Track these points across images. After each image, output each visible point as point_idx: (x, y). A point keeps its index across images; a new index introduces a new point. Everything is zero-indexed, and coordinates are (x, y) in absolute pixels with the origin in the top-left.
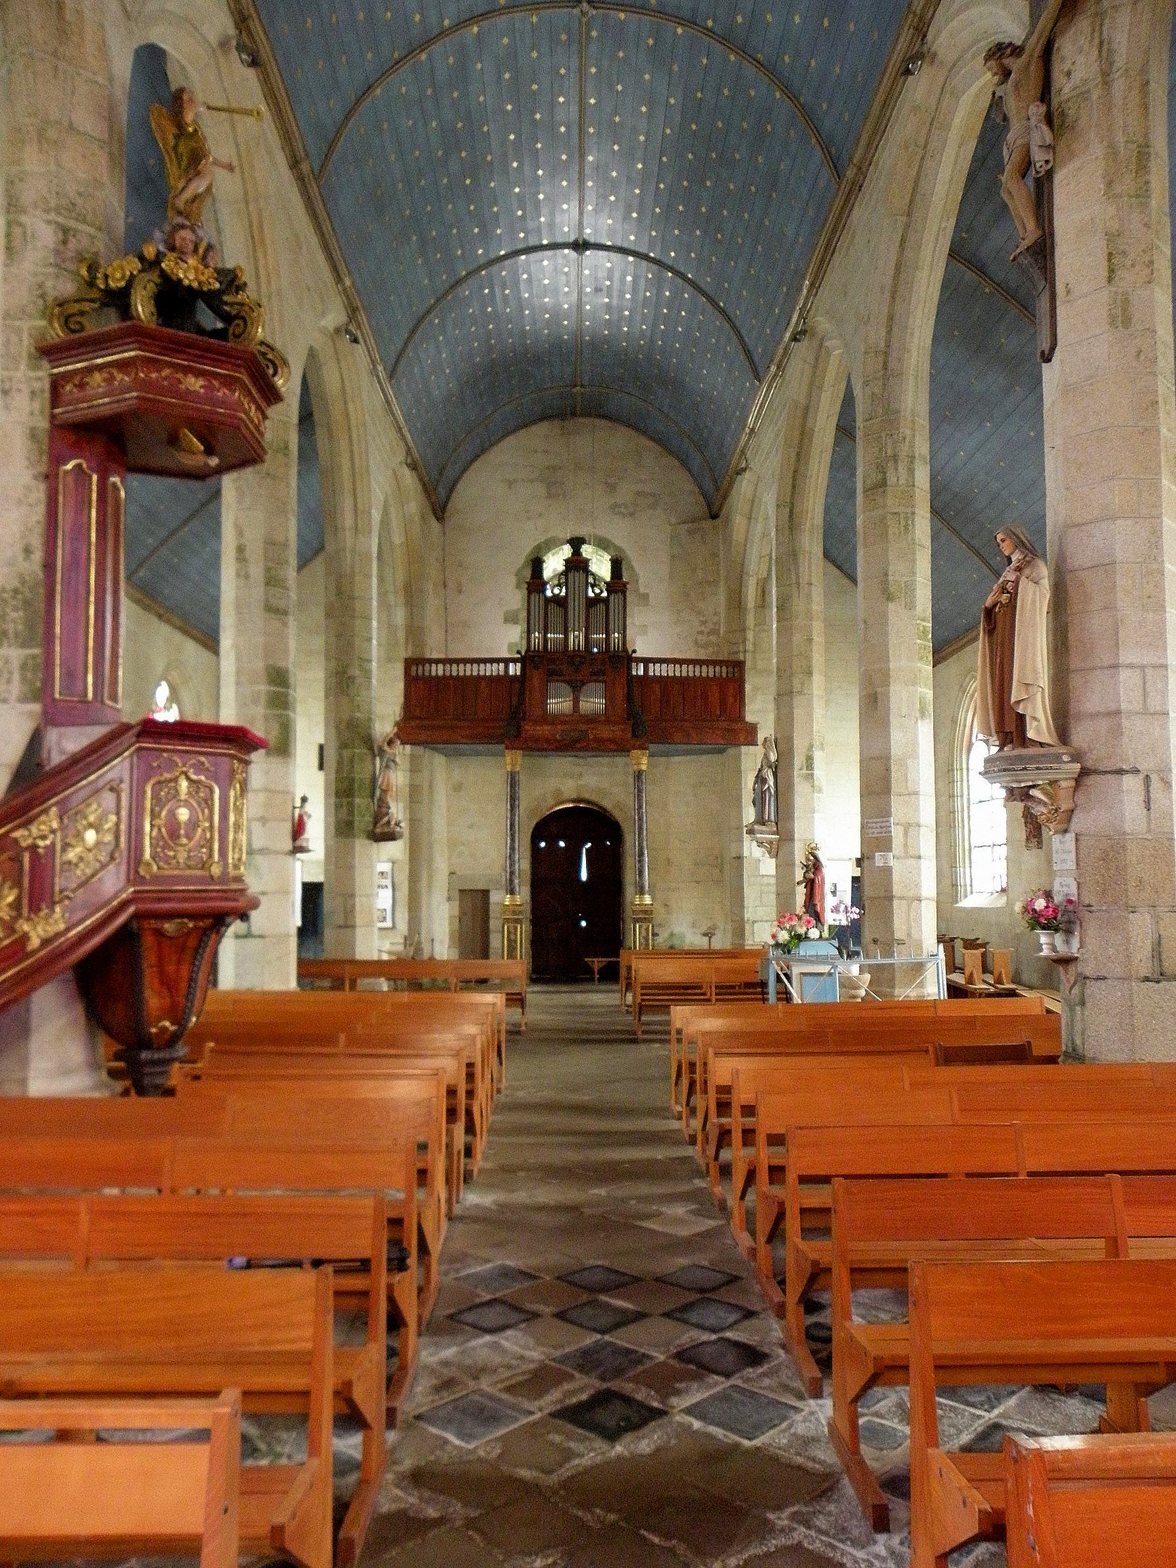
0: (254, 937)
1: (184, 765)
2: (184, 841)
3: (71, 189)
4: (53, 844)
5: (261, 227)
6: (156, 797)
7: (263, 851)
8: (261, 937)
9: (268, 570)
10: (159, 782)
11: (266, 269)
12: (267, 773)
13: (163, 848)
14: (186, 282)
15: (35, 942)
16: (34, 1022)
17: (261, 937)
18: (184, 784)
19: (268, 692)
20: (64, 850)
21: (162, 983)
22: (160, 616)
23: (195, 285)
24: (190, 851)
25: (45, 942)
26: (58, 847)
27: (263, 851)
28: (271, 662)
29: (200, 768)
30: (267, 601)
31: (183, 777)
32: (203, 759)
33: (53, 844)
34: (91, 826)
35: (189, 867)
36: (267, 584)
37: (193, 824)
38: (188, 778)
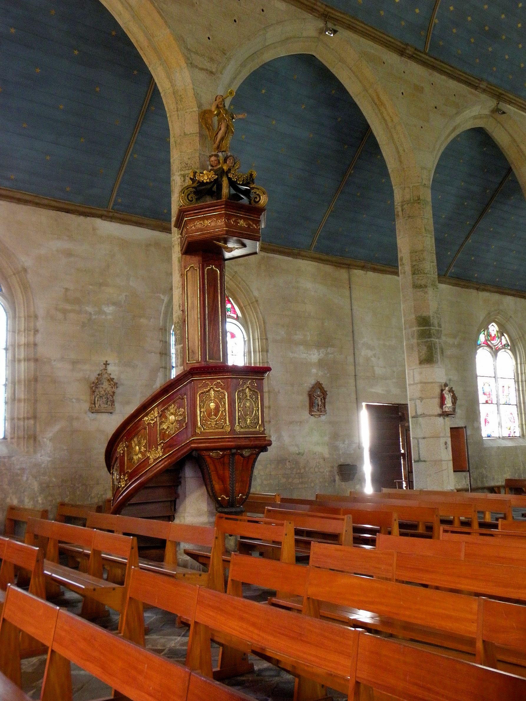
0: (422, 461)
1: (212, 385)
2: (214, 417)
3: (185, 159)
4: (156, 422)
5: (379, 98)
6: (201, 401)
7: (423, 415)
8: (424, 461)
9: (413, 266)
10: (202, 393)
11: (388, 114)
12: (421, 373)
13: (206, 420)
14: (205, 181)
15: (151, 461)
16: (187, 493)
17: (424, 461)
18: (212, 392)
19: (418, 331)
20: (161, 424)
21: (219, 478)
22: (477, 289)
23: (208, 181)
24: (216, 421)
25: (155, 460)
26: (158, 423)
27: (423, 415)
28: (419, 314)
29: (218, 385)
30: (414, 282)
31: (212, 389)
32: (219, 381)
33: (156, 422)
34: (172, 414)
35: (217, 428)
36: (414, 274)
37: (217, 409)
38: (214, 390)
